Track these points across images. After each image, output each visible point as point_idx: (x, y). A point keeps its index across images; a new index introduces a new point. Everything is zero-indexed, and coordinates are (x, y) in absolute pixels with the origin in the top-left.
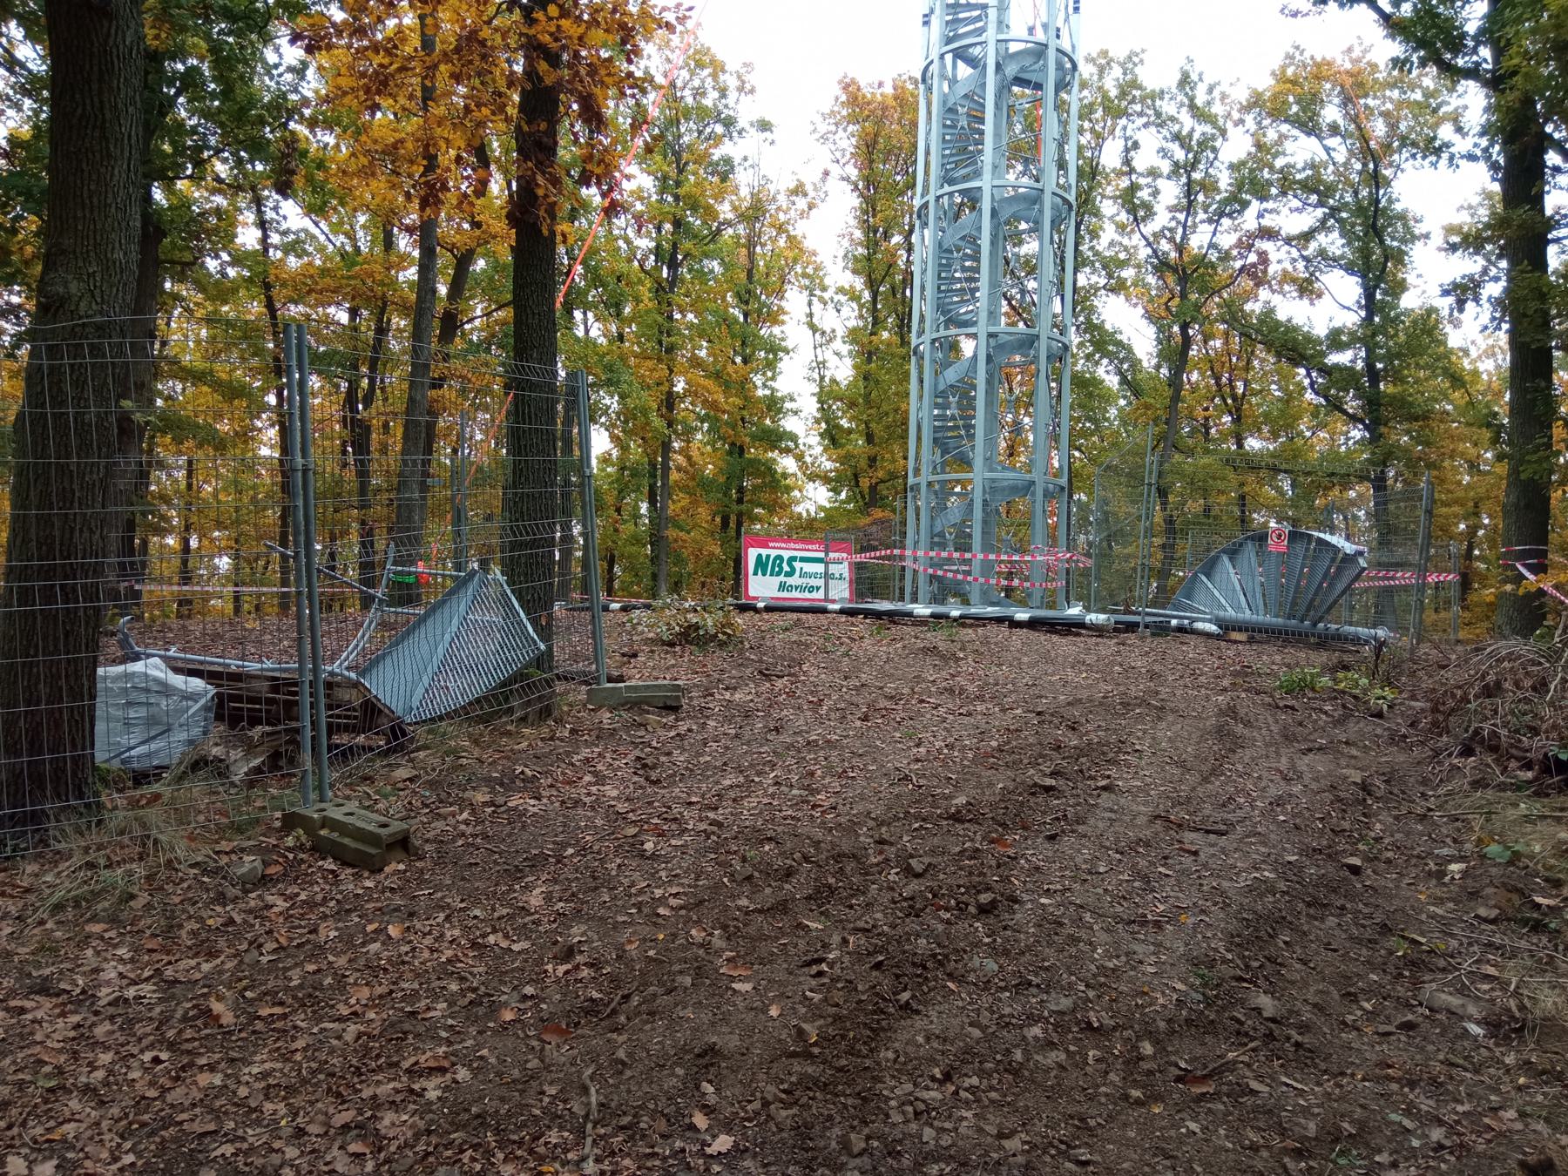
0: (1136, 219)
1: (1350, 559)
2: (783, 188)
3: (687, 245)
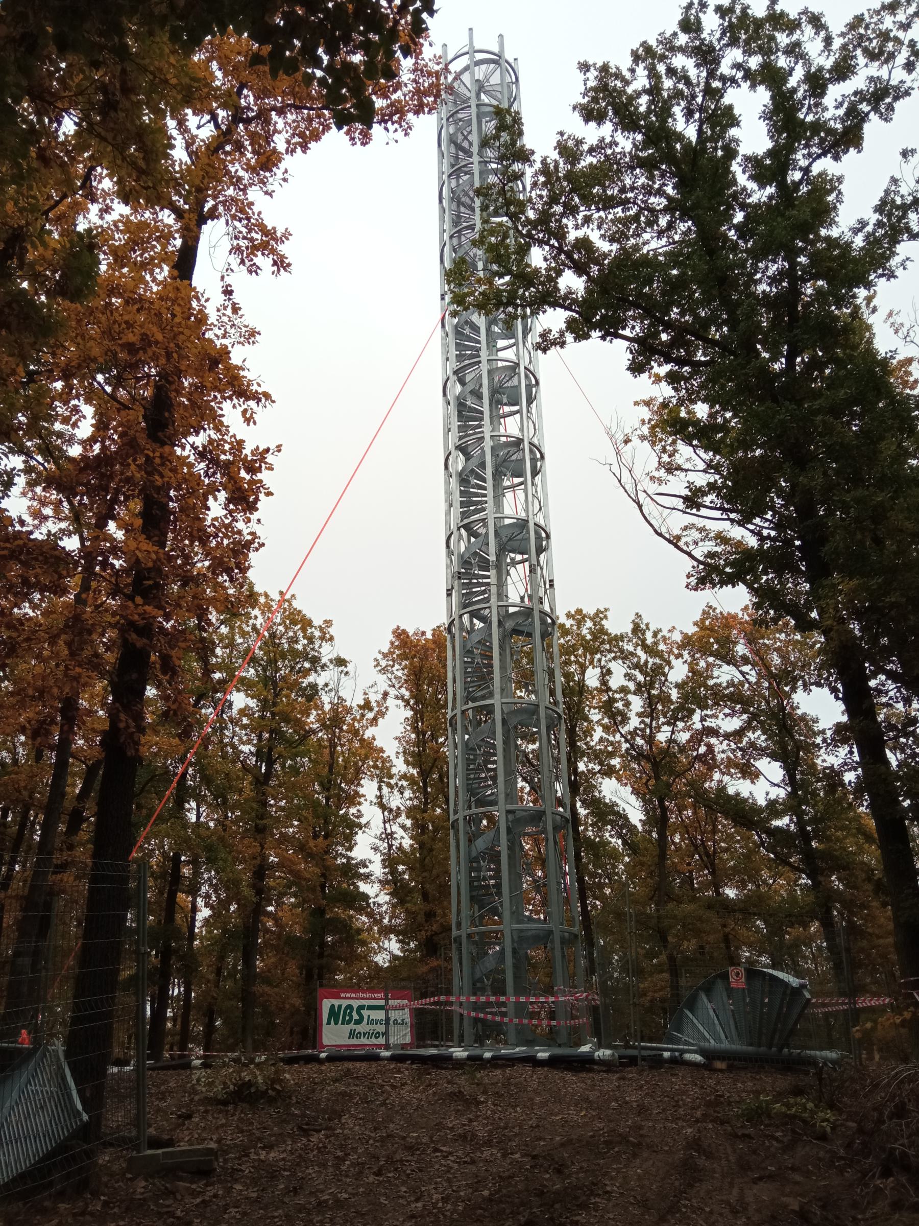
0: (615, 723)
1: (797, 992)
2: (354, 705)
3: (280, 748)
